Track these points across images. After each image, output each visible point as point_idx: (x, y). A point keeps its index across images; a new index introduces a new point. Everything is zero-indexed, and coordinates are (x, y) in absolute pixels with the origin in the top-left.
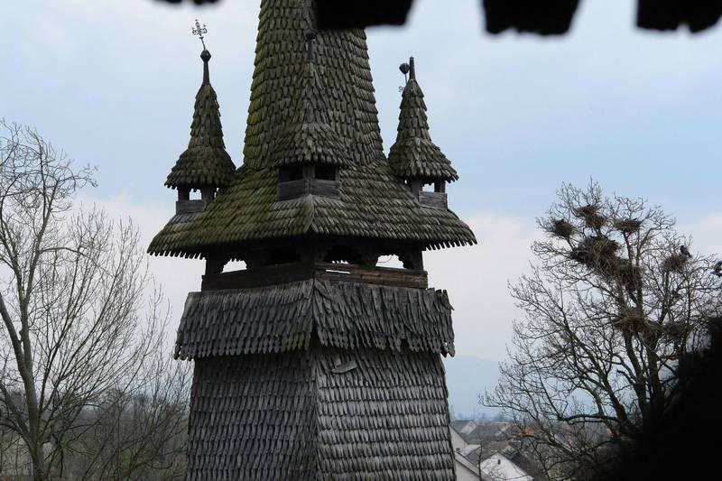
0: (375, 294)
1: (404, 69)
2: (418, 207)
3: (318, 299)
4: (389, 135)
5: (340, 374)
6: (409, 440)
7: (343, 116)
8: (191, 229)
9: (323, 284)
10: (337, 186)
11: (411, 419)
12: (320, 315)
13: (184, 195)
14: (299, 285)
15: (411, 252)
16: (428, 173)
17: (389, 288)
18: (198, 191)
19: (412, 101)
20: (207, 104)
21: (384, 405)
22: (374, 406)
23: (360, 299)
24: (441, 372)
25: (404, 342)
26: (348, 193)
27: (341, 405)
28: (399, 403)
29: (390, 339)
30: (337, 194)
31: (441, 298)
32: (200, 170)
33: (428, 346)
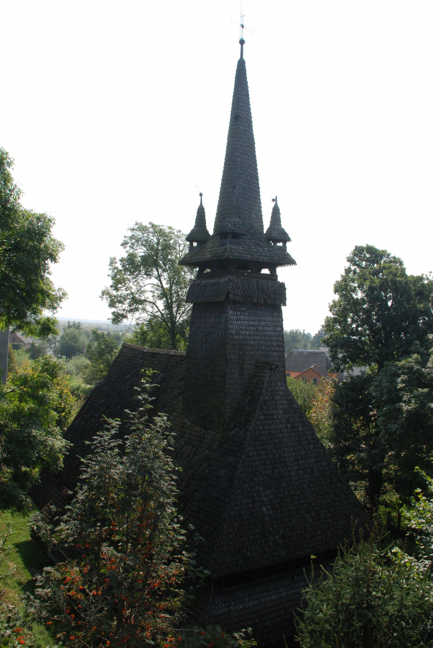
0: (255, 282)
1: (273, 200)
2: (274, 250)
3: (230, 283)
4: (266, 224)
5: (238, 311)
6: (266, 336)
7: (247, 216)
8: (192, 257)
9: (233, 277)
10: (241, 242)
11: (268, 328)
12: (231, 289)
13: (191, 244)
14: (225, 278)
15: (273, 268)
16: (278, 238)
17: (261, 280)
18: (196, 243)
19: (276, 212)
20: (201, 213)
21: (256, 322)
22: (251, 323)
23: (248, 284)
24: (280, 312)
25: (265, 300)
26: (246, 245)
27: (238, 322)
28: (262, 323)
29: (259, 299)
30: (240, 245)
31: (282, 287)
32: (198, 234)
33: (275, 302)
